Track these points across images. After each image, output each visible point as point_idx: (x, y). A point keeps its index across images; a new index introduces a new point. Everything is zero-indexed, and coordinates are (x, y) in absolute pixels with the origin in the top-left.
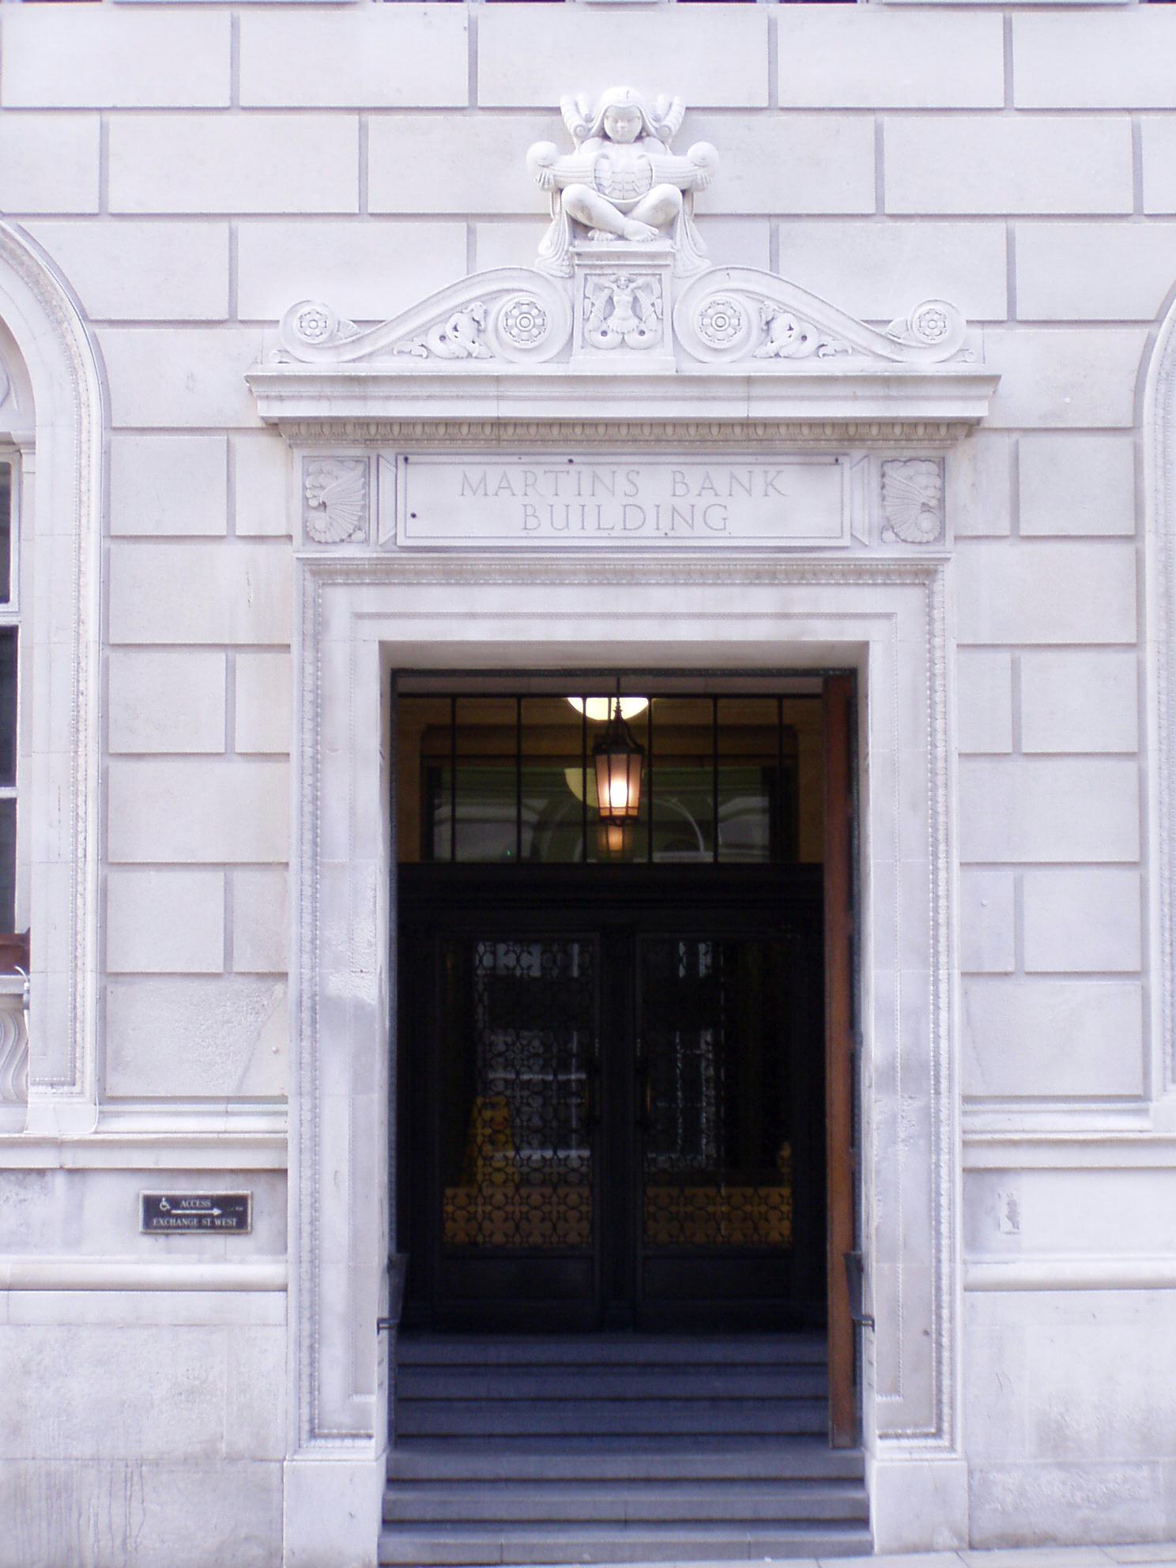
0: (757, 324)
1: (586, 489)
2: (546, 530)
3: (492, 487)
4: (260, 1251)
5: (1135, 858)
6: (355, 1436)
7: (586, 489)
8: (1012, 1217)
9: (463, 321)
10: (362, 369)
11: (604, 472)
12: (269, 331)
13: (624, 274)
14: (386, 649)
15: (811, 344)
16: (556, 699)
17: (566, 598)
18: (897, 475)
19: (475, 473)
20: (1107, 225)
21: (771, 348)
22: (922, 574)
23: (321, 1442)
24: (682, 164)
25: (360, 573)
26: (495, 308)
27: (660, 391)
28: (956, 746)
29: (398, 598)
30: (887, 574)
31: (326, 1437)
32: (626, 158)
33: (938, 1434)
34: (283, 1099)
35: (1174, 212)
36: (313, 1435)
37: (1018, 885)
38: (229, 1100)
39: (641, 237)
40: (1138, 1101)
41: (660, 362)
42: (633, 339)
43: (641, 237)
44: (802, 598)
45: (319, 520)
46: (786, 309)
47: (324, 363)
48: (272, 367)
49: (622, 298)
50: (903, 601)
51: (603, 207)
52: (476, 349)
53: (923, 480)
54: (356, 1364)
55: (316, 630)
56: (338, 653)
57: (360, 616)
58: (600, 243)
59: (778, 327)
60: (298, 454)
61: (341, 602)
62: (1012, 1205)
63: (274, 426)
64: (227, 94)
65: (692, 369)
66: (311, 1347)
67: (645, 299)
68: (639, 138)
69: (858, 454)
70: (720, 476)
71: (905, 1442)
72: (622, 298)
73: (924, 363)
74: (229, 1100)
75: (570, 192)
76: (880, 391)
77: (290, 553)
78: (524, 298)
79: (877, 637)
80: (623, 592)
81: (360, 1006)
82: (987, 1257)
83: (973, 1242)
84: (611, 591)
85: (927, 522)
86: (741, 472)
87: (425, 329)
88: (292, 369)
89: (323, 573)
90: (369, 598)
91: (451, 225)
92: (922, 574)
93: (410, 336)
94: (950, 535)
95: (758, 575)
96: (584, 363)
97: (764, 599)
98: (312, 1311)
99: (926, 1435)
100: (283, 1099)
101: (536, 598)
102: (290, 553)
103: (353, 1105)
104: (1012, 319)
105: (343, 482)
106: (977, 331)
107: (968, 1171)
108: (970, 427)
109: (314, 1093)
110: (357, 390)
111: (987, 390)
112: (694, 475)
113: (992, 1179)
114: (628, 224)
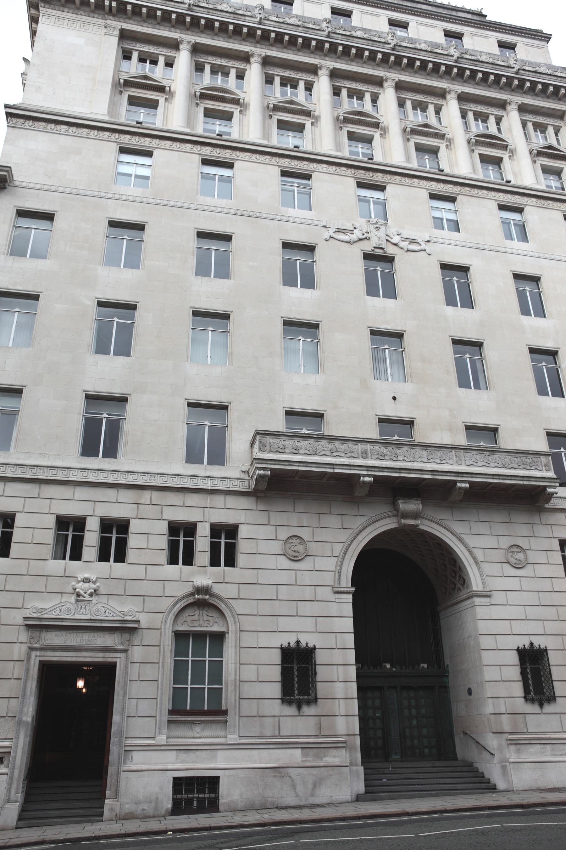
0: (104, 611)
1: (75, 636)
2: (68, 643)
3: (60, 636)
4: (4, 767)
5: (156, 697)
6: (15, 802)
7: (75, 636)
8: (132, 759)
9: (58, 609)
10: (42, 616)
11: (78, 634)
12: (28, 610)
13: (84, 603)
14: (40, 661)
15: (111, 615)
16: (549, 181)
17: (70, 654)
18: (124, 635)
19: (57, 633)
20: (159, 598)
21: (105, 615)
22: (126, 651)
23: (9, 804)
24: (94, 586)
25: (37, 649)
26: (63, 607)
27: (88, 621)
28: (129, 679)
29: (43, 653)
30: (121, 651)
31: (10, 802)
32: (86, 585)
33: (116, 798)
34: (12, 739)
35: (2, 299)
36: (8, 802)
37: (137, 702)
38: (3, 739)
39: (87, 597)
40: (153, 738)
41: (88, 617)
42: (84, 613)
43: (87, 597)
44: (107, 655)
45: (32, 640)
46: (108, 609)
47: (35, 615)
48: (28, 616)
49: (83, 607)
50: (123, 655)
51: (82, 592)
52: (60, 614)
53: (127, 636)
54: (17, 789)
55: (29, 658)
56: (32, 662)
57: (36, 656)
58: (81, 598)
59: (107, 612)
60: (30, 630)
61: (34, 654)
62: (132, 756)
63: (27, 625)
64: (179, 577)
65: (93, 618)
66: (10, 785)
67: (87, 607)
68: (89, 582)
69: (117, 632)
70: (96, 635)
71: (110, 800)
72: (83, 607)
73: (129, 618)
74: (3, 739)
75: (77, 590)
76: (121, 622)
77: (27, 645)
78: (68, 606)
79: (118, 661)
80: (79, 653)
81: (27, 722)
82: (127, 766)
83: (125, 763)
84: (77, 653)
85: (127, 643)
86: (99, 634)
87: (52, 610)
88: (31, 616)
89: (31, 649)
90: (38, 653)
91: (59, 594)
92: (126, 651)
93: (50, 611)
94: (131, 645)
95: (101, 650)
96: (77, 616)
97: (101, 655)
98: (11, 778)
99: (114, 799)
100: (12, 739)
101: (65, 654)
102: (27, 645)
103: (24, 740)
104: (143, 612)
105: (36, 634)
106: (138, 613)
107: (125, 750)
108: (135, 628)
109: (18, 737)
110: (40, 620)
111: (138, 623)
112: (92, 635)
113: (128, 752)
114: (86, 595)
